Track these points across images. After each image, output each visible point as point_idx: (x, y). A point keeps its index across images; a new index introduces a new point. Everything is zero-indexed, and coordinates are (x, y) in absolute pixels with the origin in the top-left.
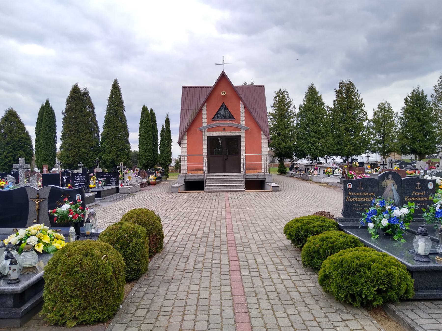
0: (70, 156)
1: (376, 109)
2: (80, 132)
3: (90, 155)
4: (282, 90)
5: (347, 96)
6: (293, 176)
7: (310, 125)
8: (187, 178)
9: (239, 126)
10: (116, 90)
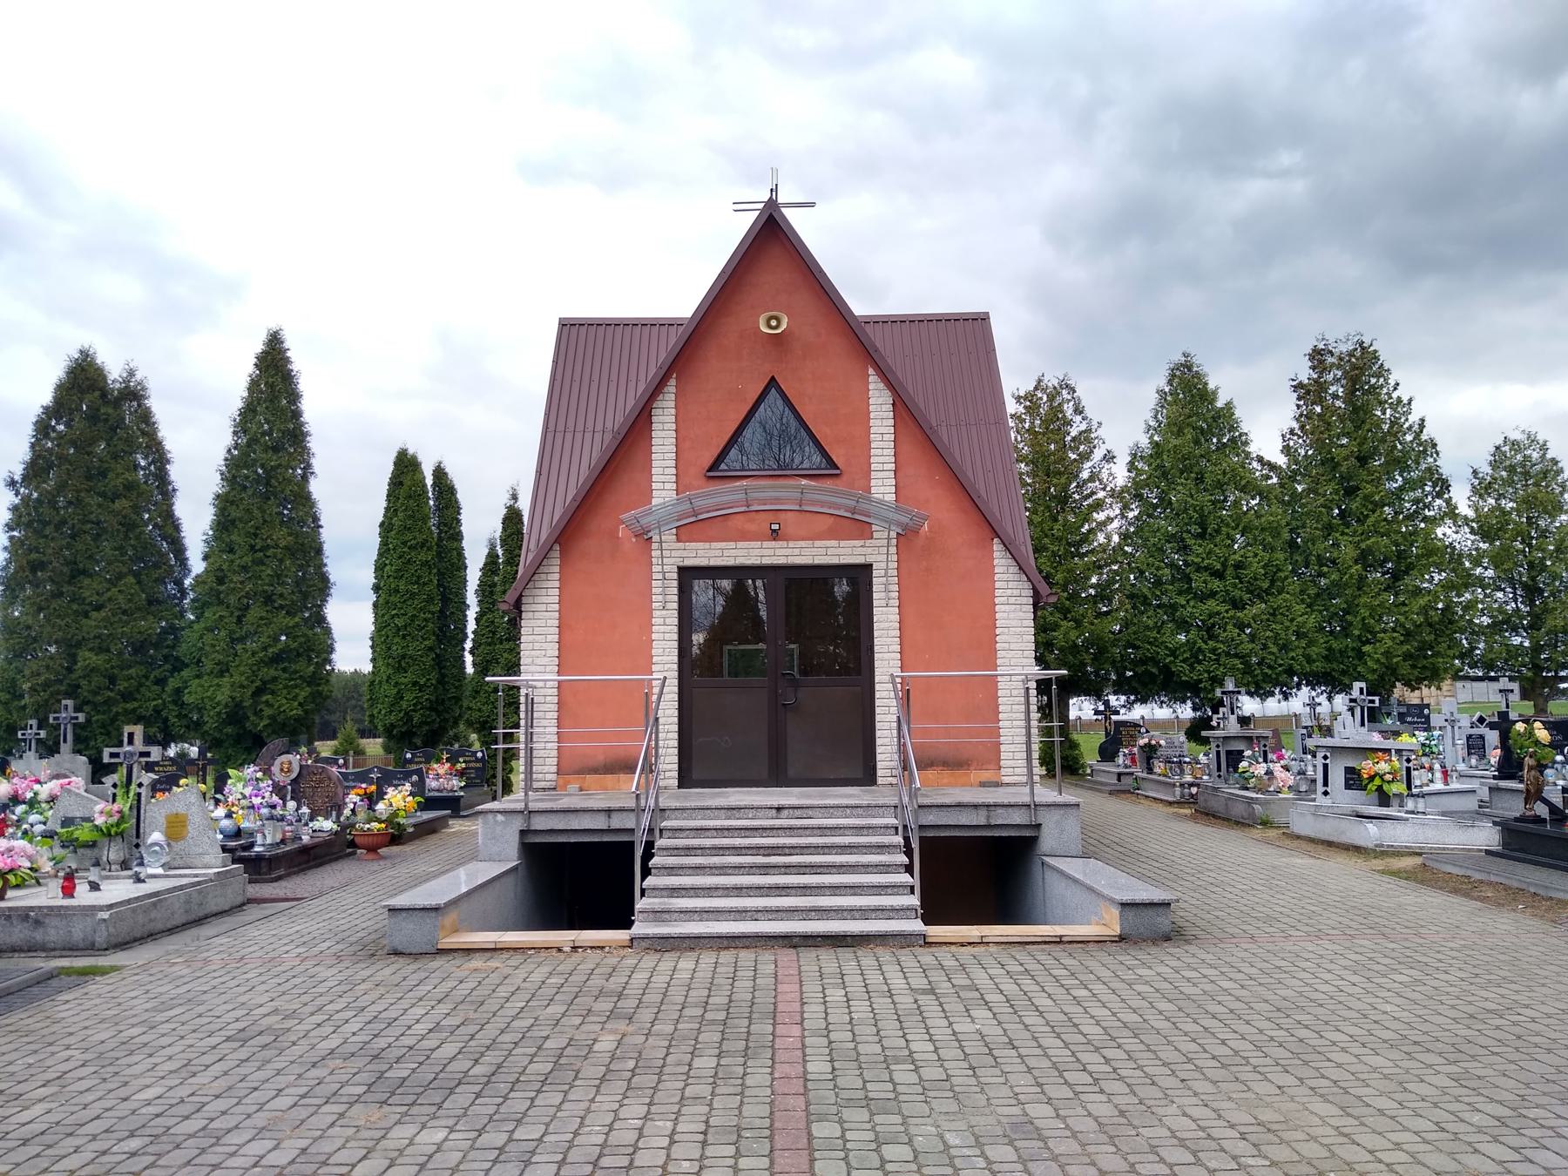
0: (26, 686)
1: (1486, 469)
2: (84, 572)
3: (122, 686)
4: (1051, 381)
5: (1350, 403)
6: (1125, 789)
7: (1190, 542)
8: (539, 823)
9: (869, 513)
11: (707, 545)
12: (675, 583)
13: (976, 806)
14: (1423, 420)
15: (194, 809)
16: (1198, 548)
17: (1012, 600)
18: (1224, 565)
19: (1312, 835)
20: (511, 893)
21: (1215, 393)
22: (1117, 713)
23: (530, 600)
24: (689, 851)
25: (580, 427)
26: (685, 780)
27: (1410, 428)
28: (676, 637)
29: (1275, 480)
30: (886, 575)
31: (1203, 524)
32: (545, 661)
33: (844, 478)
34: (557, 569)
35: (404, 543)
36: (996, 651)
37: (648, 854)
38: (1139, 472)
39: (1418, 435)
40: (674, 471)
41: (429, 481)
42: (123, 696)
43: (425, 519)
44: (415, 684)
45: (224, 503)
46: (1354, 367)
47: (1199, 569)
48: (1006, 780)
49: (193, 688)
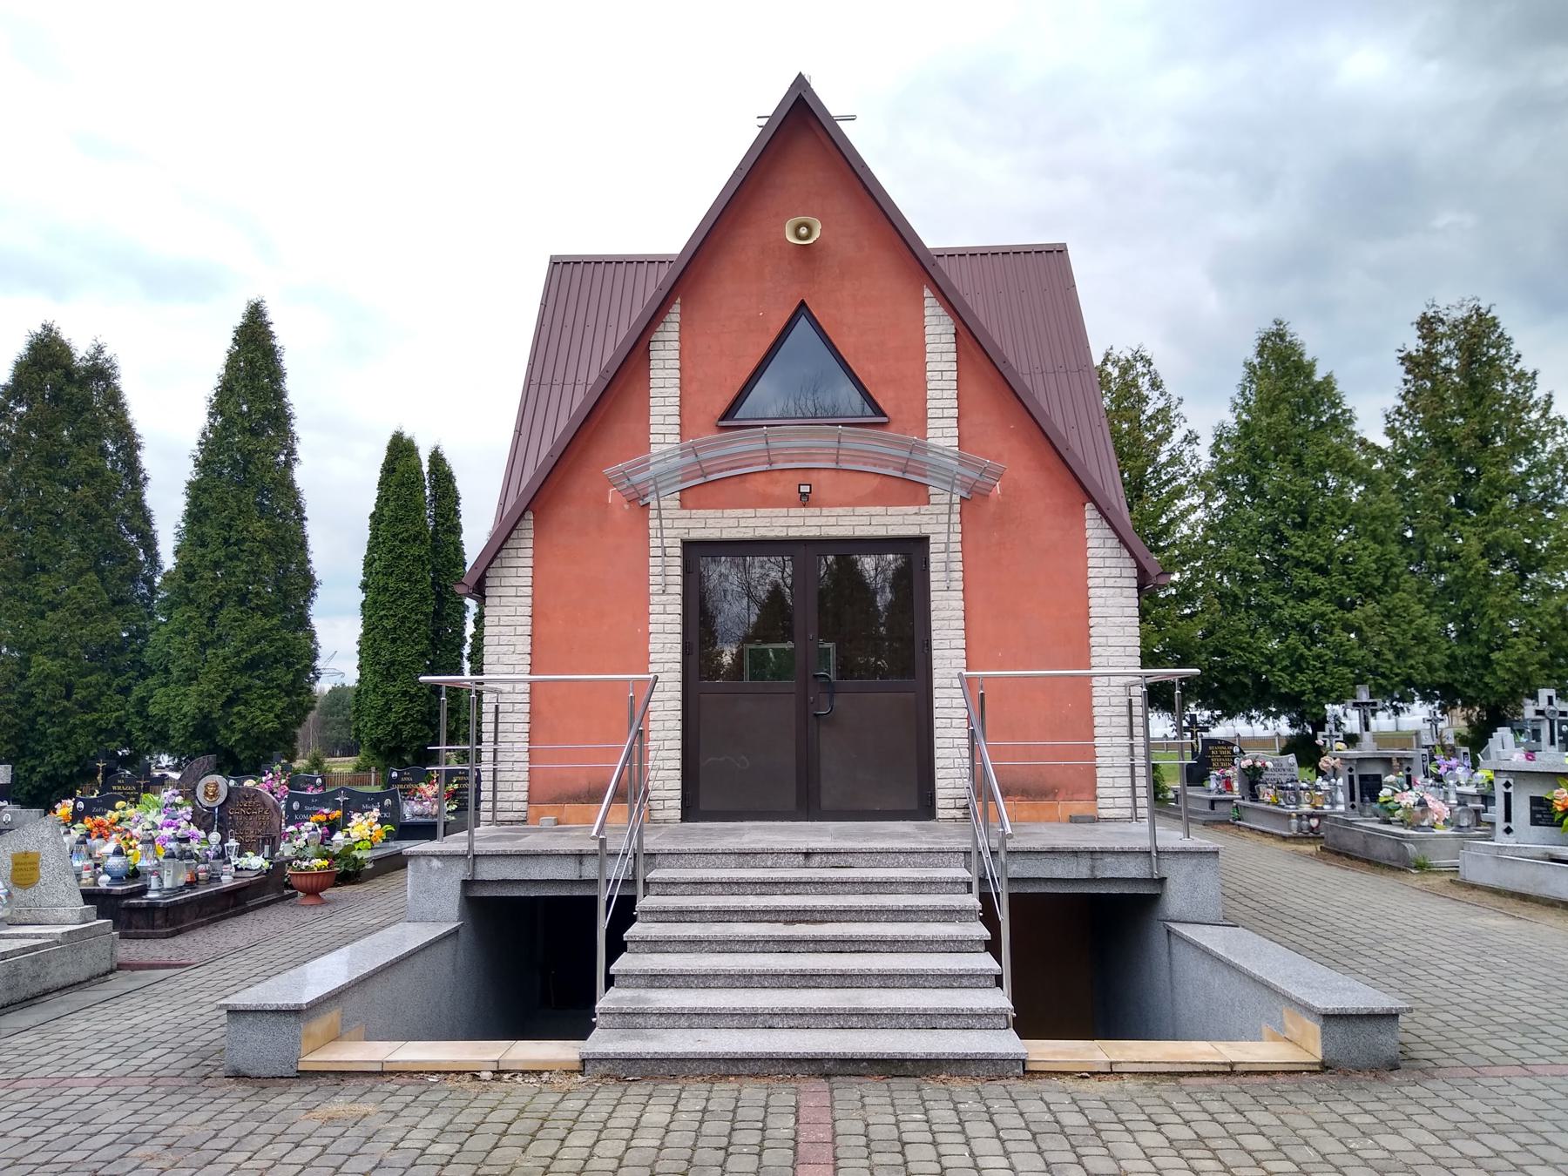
3: (79, 695)
7: (1288, 533)
8: (488, 871)
10: (255, 356)
11: (718, 513)
12: (679, 561)
13: (1075, 853)
14: (1550, 396)
15: (48, 847)
16: (1300, 540)
17: (1110, 582)
18: (1329, 559)
19: (1496, 884)
20: (446, 970)
21: (1312, 365)
22: (1206, 730)
23: (496, 582)
24: (682, 915)
25: (570, 379)
26: (691, 810)
27: (1536, 404)
28: (679, 629)
29: (1379, 465)
30: (946, 551)
31: (1303, 514)
32: (514, 659)
33: (893, 427)
34: (530, 543)
35: (395, 536)
36: (1089, 647)
37: (625, 912)
38: (1224, 457)
39: (1546, 411)
40: (677, 420)
41: (425, 469)
42: (81, 706)
43: (419, 509)
44: (405, 693)
45: (196, 491)
46: (1472, 335)
47: (1298, 563)
48: (1104, 813)
49: (157, 698)
